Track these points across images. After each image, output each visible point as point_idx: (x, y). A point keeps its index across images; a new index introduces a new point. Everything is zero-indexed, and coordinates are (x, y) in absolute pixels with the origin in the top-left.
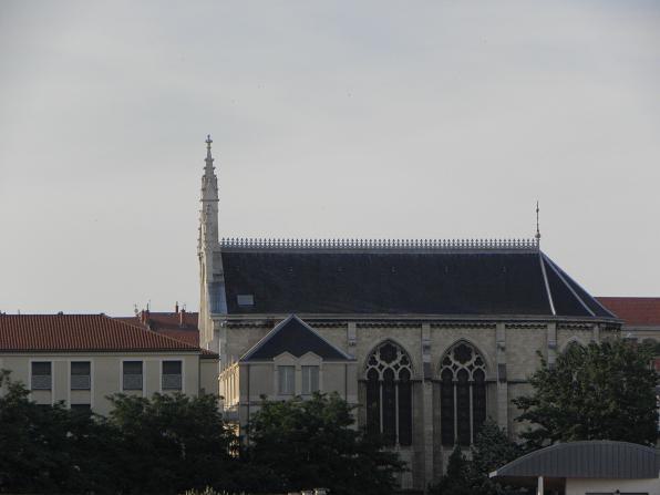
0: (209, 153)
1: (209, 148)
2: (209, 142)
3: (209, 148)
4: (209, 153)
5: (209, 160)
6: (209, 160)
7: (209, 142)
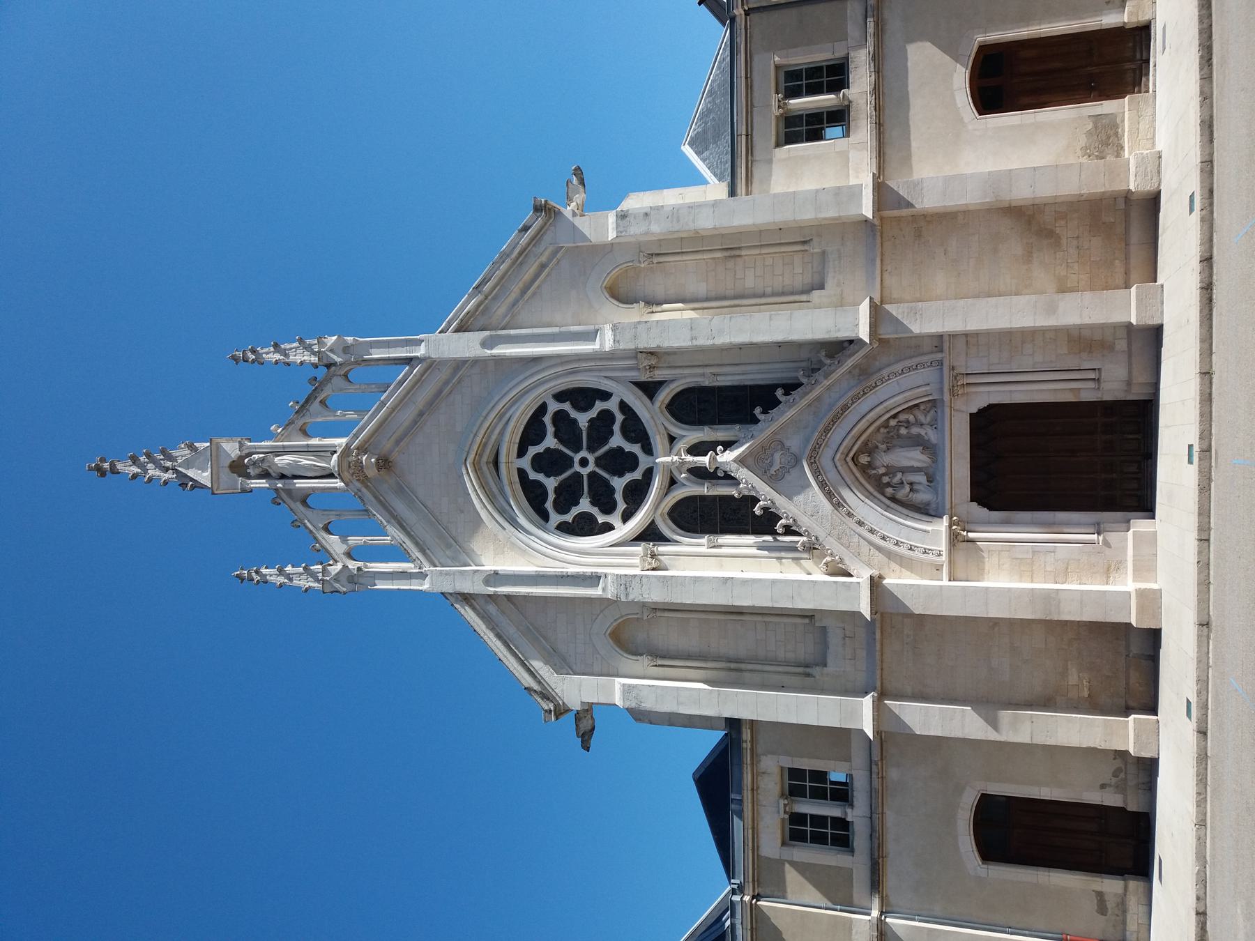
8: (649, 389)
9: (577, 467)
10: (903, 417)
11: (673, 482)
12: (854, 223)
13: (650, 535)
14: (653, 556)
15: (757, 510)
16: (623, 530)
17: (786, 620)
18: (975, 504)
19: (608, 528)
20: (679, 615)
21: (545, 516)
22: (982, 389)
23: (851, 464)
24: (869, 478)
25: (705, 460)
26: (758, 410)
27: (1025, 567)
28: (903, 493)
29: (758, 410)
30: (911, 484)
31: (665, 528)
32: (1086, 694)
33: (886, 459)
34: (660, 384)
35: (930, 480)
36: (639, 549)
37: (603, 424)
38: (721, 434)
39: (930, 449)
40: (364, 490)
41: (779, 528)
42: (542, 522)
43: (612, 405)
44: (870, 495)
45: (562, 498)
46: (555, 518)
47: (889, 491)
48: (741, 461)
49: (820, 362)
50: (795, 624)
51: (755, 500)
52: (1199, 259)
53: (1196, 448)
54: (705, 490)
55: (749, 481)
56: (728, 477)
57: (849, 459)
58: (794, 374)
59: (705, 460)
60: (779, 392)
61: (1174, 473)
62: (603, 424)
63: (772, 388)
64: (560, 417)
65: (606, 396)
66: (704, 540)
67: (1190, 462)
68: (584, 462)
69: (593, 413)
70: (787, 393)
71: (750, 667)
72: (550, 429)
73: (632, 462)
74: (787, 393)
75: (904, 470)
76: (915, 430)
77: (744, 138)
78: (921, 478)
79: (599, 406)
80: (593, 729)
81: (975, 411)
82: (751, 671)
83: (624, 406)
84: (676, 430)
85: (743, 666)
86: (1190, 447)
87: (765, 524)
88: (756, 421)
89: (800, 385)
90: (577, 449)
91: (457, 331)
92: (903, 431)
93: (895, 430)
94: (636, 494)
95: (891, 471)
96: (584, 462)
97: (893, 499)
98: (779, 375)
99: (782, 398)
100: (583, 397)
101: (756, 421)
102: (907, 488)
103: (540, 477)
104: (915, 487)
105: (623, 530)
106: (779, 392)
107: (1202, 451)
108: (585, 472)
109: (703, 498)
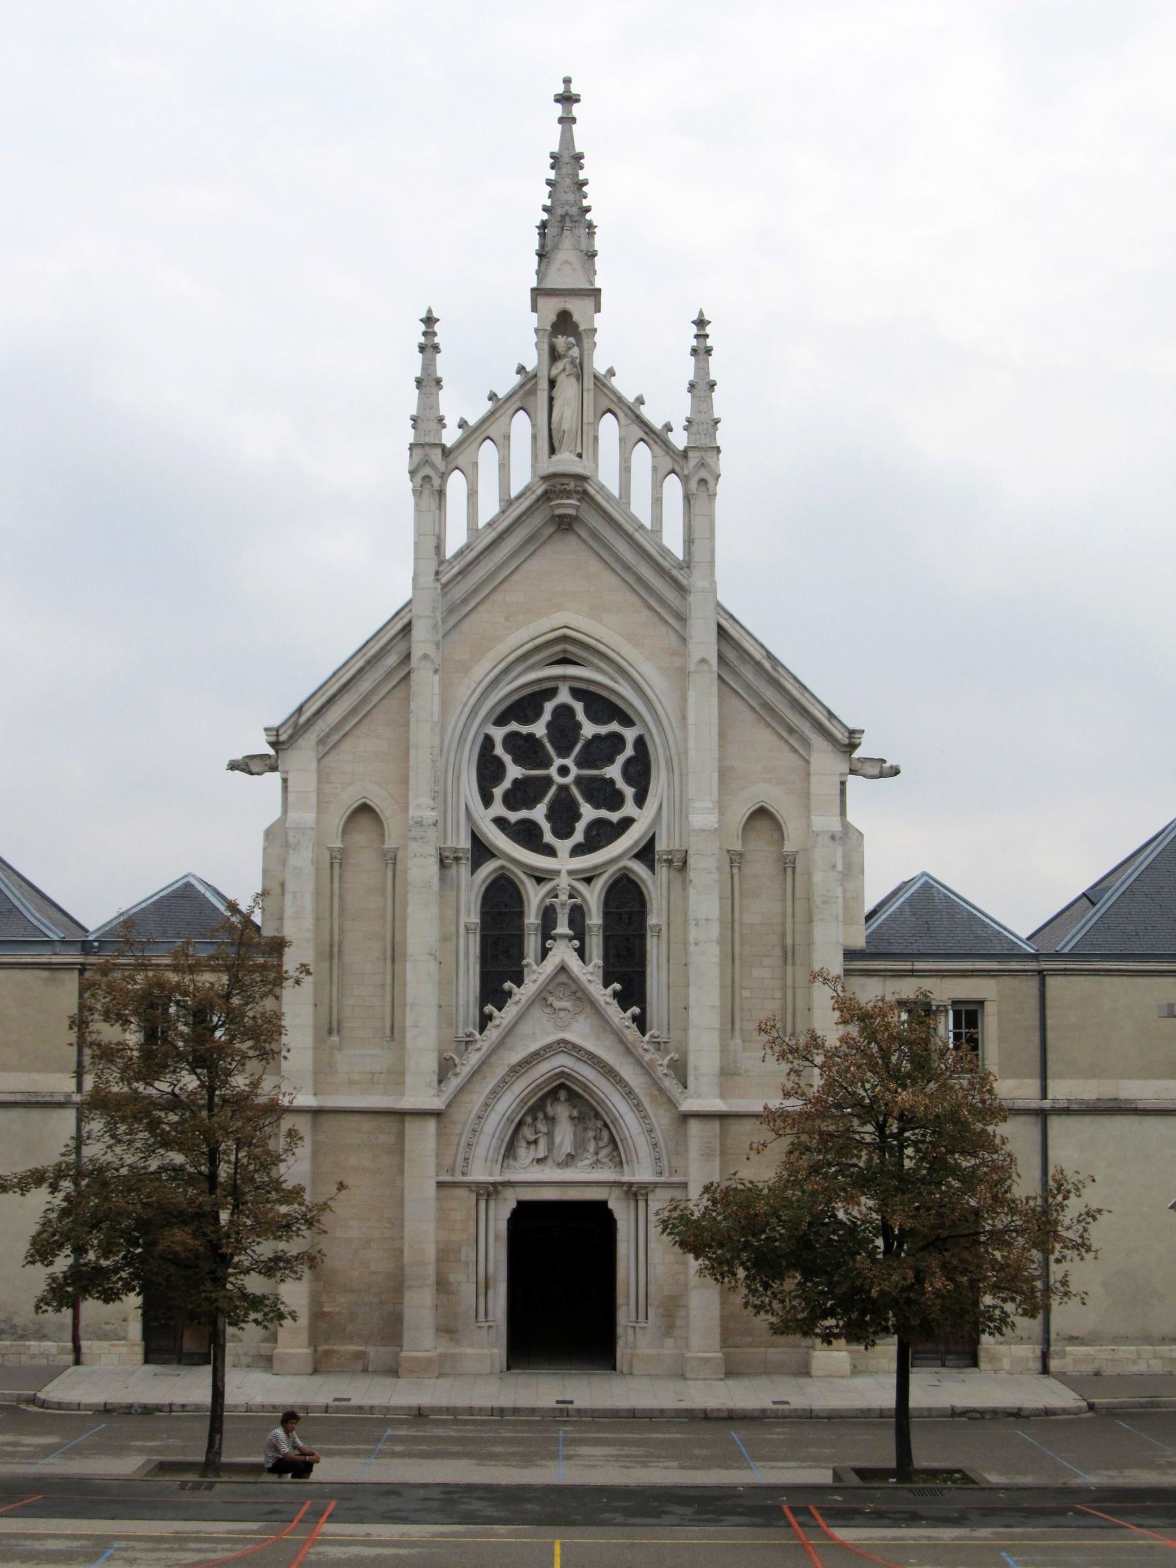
0: (567, 139)
1: (567, 121)
2: (567, 99)
3: (567, 121)
4: (567, 139)
5: (567, 163)
6: (567, 163)
7: (567, 99)
8: (646, 853)
9: (558, 762)
10: (605, 1134)
11: (540, 879)
12: (330, 1372)
13: (481, 851)
14: (457, 859)
15: (508, 985)
16: (485, 819)
17: (388, 1009)
18: (514, 1205)
19: (487, 800)
20: (389, 888)
21: (500, 721)
22: (632, 1217)
23: (558, 1082)
24: (543, 1099)
25: (563, 928)
26: (617, 986)
27: (836, 1501)
28: (527, 1132)
29: (617, 986)
30: (535, 1142)
31: (488, 868)
32: (326, 1309)
33: (562, 1111)
34: (652, 868)
35: (539, 1161)
36: (465, 843)
37: (607, 796)
38: (595, 945)
39: (571, 1159)
40: (534, 497)
41: (489, 1008)
42: (494, 717)
43: (629, 808)
44: (523, 1102)
45: (521, 742)
46: (498, 734)
47: (529, 1120)
48: (563, 969)
49: (667, 1052)
50: (383, 1019)
51: (519, 982)
52: (718, 497)
53: (570, 1406)
54: (532, 918)
55: (538, 973)
56: (545, 952)
57: (563, 1080)
58: (655, 1023)
59: (563, 928)
60: (636, 1010)
61: (544, 1389)
62: (607, 796)
63: (641, 1001)
64: (617, 741)
65: (640, 800)
66: (475, 919)
67: (558, 1402)
68: (564, 771)
69: (621, 784)
70: (635, 1018)
71: (335, 968)
72: (603, 730)
73: (562, 831)
74: (635, 1018)
75: (550, 1135)
76: (592, 1147)
77: (910, 967)
78: (541, 1152)
79: (629, 792)
80: (252, 774)
81: (611, 1205)
82: (331, 969)
83: (627, 822)
84: (600, 884)
85: (336, 960)
86: (572, 1402)
87: (493, 992)
88: (606, 986)
89: (643, 1033)
90: (580, 764)
91: (720, 628)
92: (591, 1134)
93: (589, 1114)
94: (527, 835)
95: (551, 1120)
96: (564, 771)
97: (520, 1124)
98: (655, 1006)
99: (629, 1013)
100: (640, 772)
101: (606, 986)
102: (532, 1138)
103: (547, 716)
104: (533, 1147)
105: (485, 819)
106: (636, 1010)
107: (568, 1410)
108: (553, 771)
109: (521, 915)
